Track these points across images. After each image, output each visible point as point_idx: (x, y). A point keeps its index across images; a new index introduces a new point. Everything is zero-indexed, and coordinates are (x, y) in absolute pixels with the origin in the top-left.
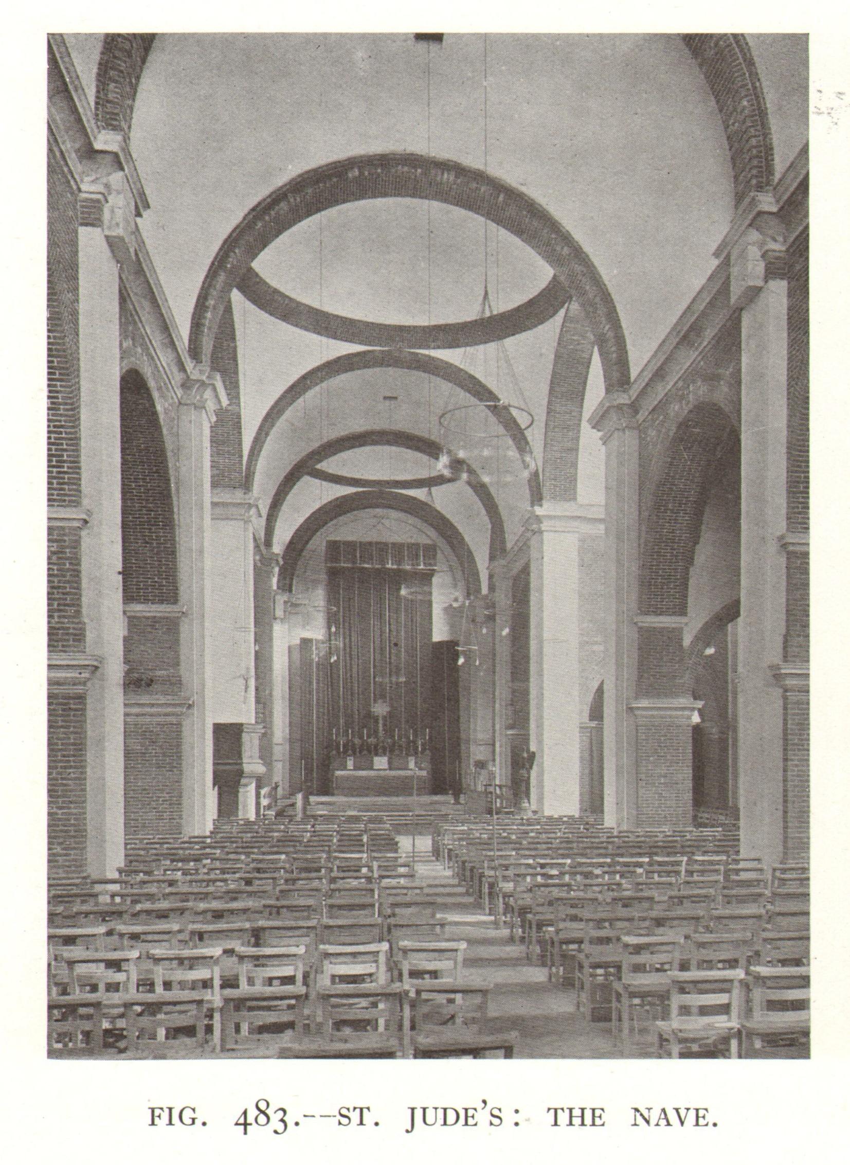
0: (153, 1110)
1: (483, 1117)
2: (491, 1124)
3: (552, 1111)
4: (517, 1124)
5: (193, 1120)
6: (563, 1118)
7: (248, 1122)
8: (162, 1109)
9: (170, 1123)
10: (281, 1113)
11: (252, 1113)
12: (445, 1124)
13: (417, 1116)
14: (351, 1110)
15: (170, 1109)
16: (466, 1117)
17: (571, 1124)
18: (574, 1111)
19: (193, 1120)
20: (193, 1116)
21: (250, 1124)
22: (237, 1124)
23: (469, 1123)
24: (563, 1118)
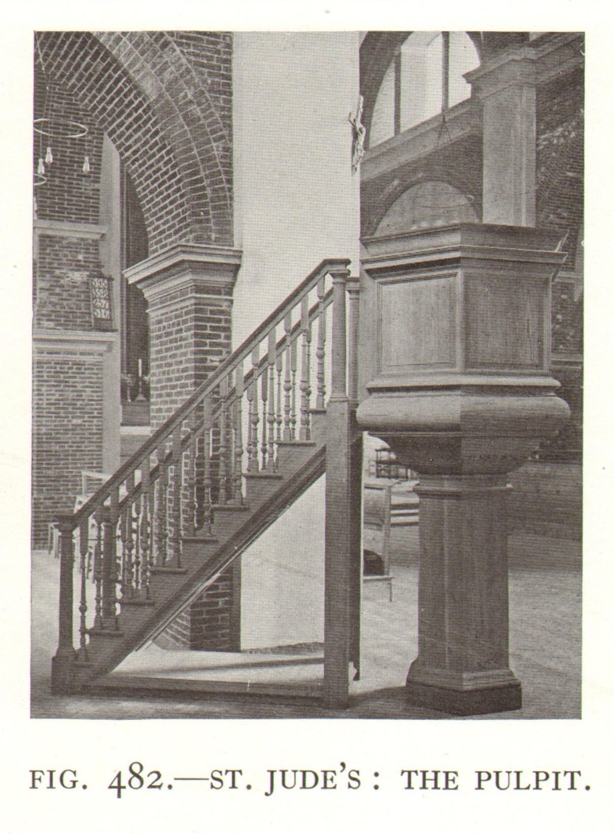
0: (33, 772)
1: (342, 779)
2: (350, 786)
3: (406, 774)
4: (588, 788)
5: (74, 782)
6: (417, 780)
7: (122, 784)
8: (334, 772)
9: (51, 786)
10: (155, 776)
11: (126, 776)
12: (304, 786)
13: (277, 779)
14: (224, 772)
15: (51, 772)
16: (325, 780)
17: (424, 787)
18: (427, 774)
19: (74, 782)
20: (75, 779)
21: (124, 787)
22: (110, 787)
23: (450, 786)
24: (417, 780)
